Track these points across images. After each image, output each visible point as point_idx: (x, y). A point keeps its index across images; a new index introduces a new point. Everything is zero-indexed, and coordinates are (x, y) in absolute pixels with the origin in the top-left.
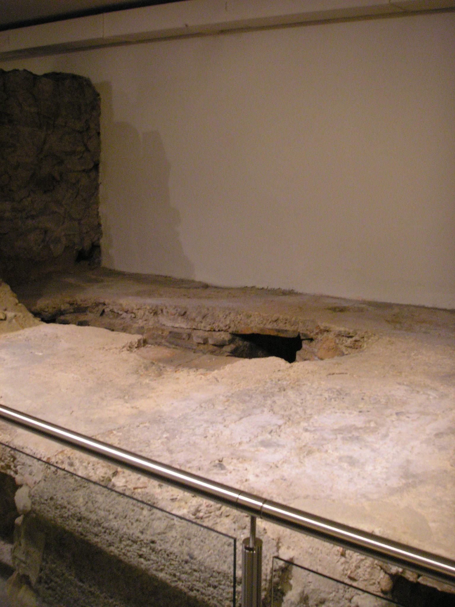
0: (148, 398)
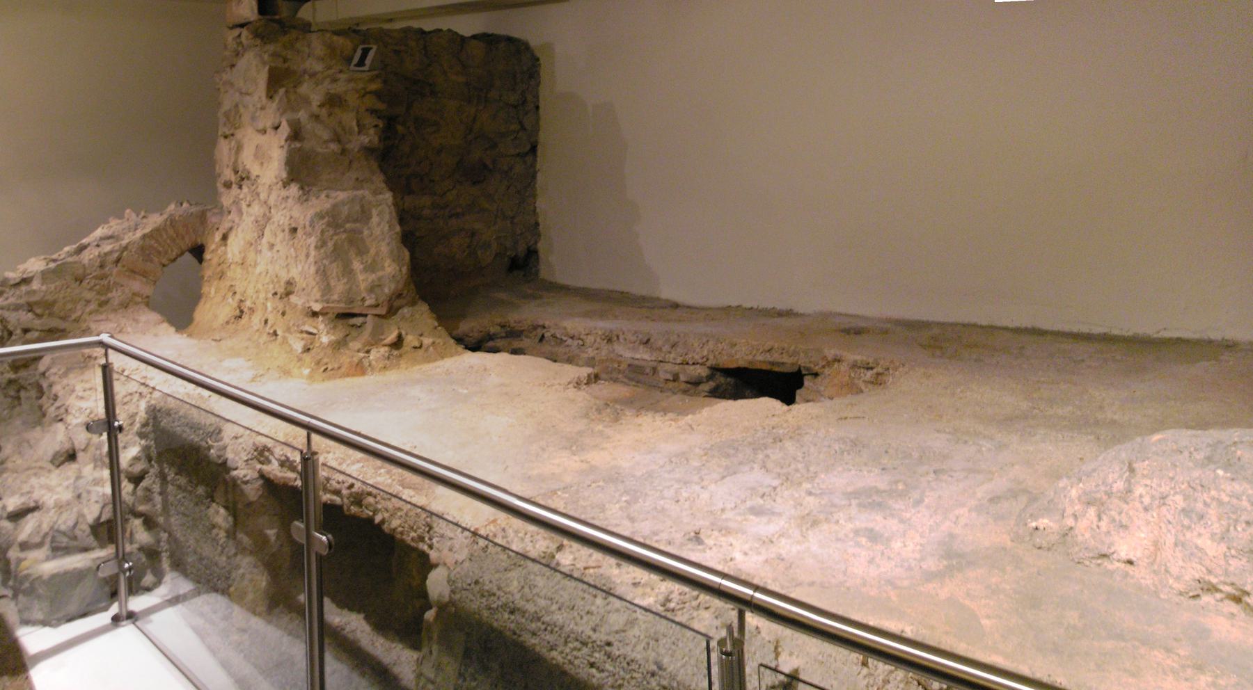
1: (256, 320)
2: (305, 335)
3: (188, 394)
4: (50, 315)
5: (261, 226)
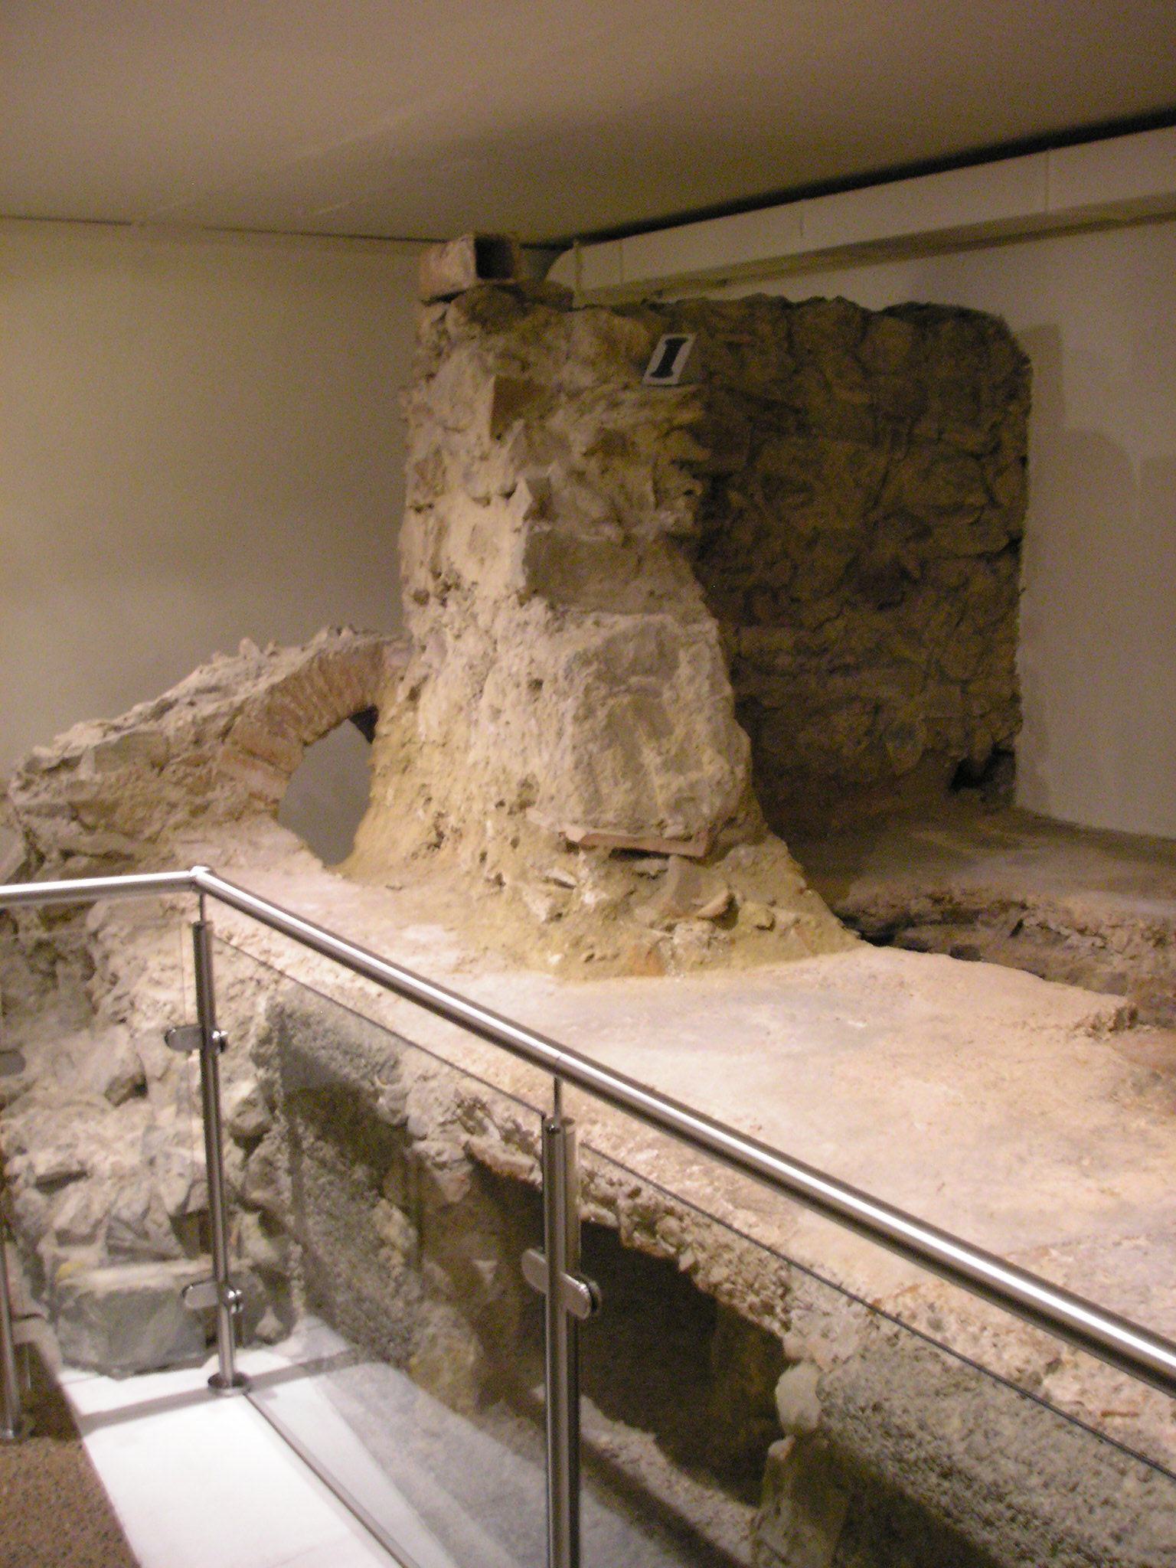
0: (1145, 1170)
1: (466, 852)
2: (553, 888)
3: (341, 988)
4: (109, 827)
5: (479, 674)
